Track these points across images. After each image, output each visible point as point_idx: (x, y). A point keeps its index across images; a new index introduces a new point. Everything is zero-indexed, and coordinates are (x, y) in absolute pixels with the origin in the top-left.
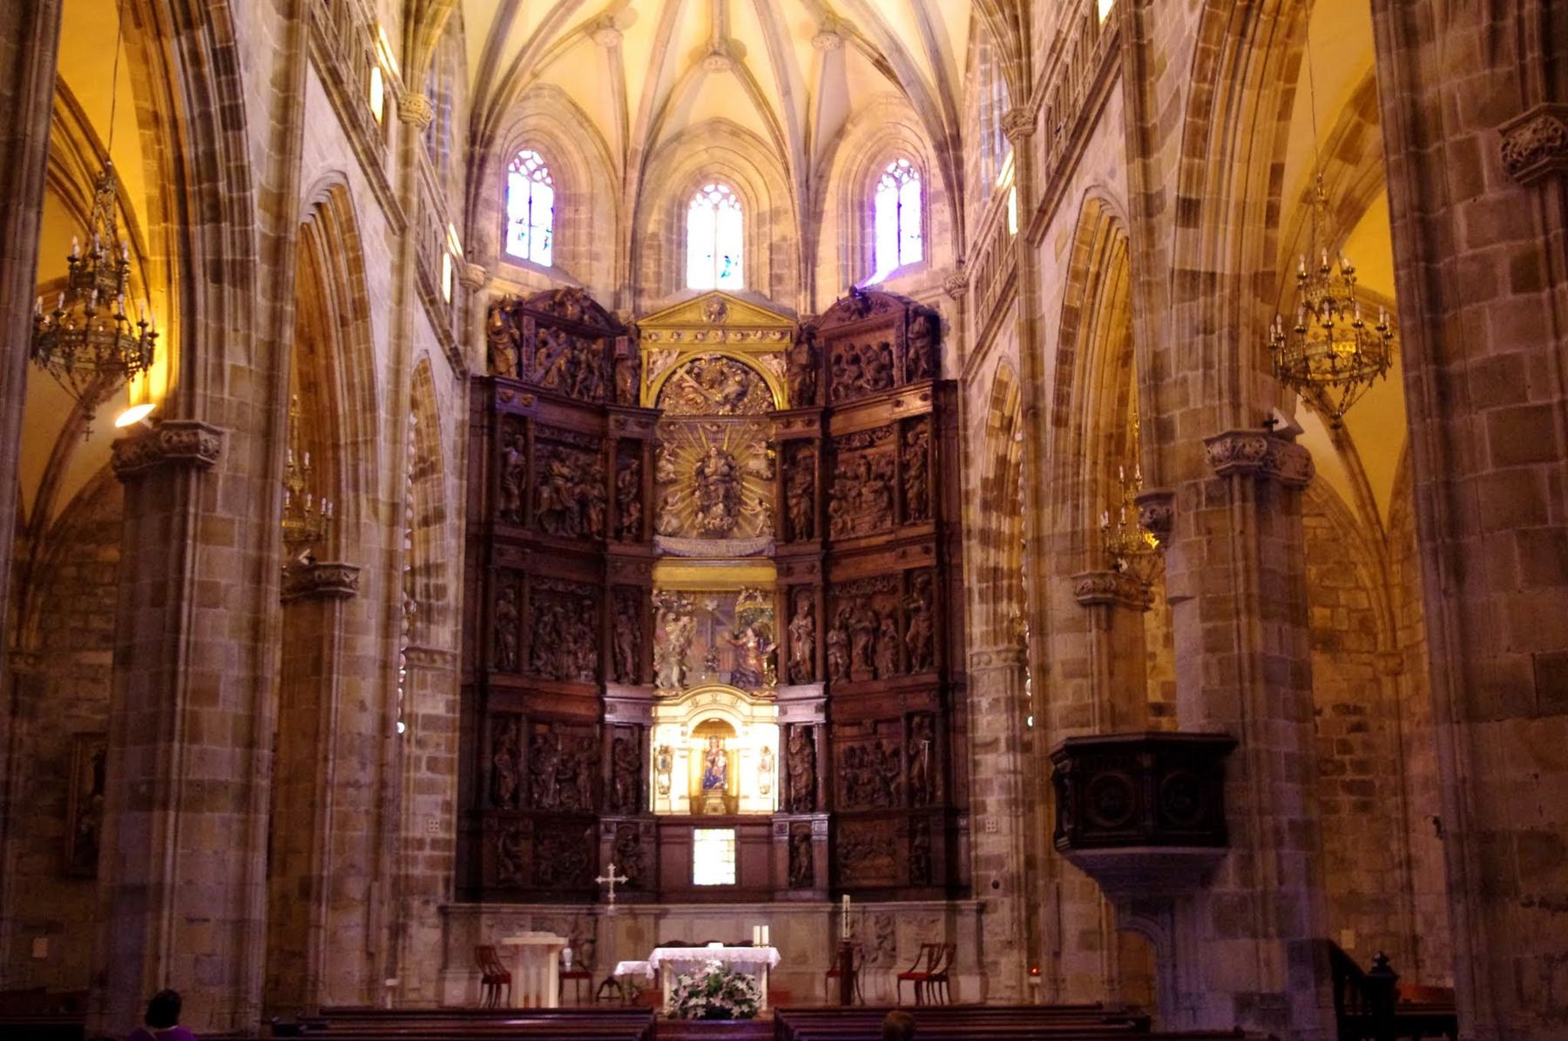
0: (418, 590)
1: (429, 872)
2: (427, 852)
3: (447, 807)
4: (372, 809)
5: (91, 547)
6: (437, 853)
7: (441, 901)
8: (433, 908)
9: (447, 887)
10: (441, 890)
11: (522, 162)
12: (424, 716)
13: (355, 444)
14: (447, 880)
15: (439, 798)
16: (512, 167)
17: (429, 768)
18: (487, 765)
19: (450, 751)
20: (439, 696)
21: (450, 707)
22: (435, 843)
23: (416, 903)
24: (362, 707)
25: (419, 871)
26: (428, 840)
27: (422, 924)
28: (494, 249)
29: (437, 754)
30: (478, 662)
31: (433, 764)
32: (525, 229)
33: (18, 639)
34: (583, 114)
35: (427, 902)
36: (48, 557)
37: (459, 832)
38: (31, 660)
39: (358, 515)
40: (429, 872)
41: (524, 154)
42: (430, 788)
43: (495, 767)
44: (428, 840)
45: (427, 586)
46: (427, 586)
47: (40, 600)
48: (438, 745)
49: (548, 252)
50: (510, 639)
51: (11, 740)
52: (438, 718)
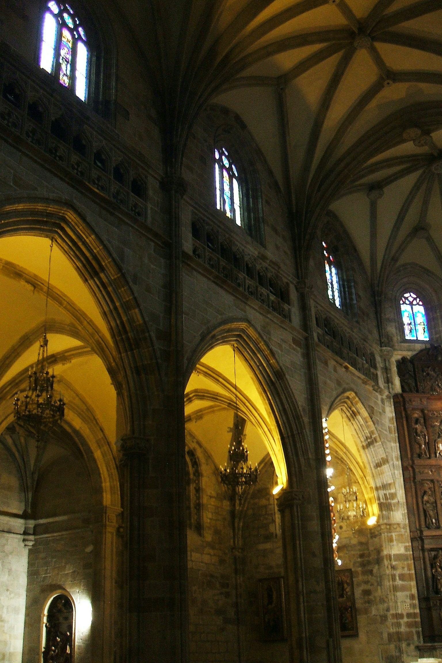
0: (381, 497)
1: (408, 630)
2: (405, 619)
3: (412, 597)
4: (325, 603)
5: (257, 500)
6: (410, 620)
7: (417, 643)
8: (412, 647)
9: (419, 637)
10: (415, 637)
11: (406, 298)
12: (394, 555)
13: (293, 435)
14: (418, 633)
15: (408, 593)
16: (401, 302)
17: (400, 579)
18: (429, 574)
19: (409, 569)
20: (400, 545)
21: (406, 548)
22: (409, 615)
23: (404, 645)
24: (314, 555)
25: (403, 629)
26: (405, 614)
27: (408, 656)
28: (396, 338)
29: (404, 572)
30: (418, 527)
31: (402, 577)
32: (413, 326)
33: (234, 542)
34: (428, 270)
35: (408, 645)
36: (241, 508)
37: (420, 609)
38: (240, 550)
39: (300, 467)
40: (408, 630)
41: (406, 295)
42: (403, 589)
43: (433, 575)
44: (405, 614)
45: (385, 495)
46: (385, 495)
47: (241, 524)
48: (403, 568)
49: (426, 334)
50: (431, 513)
51: (236, 585)
52: (401, 555)
